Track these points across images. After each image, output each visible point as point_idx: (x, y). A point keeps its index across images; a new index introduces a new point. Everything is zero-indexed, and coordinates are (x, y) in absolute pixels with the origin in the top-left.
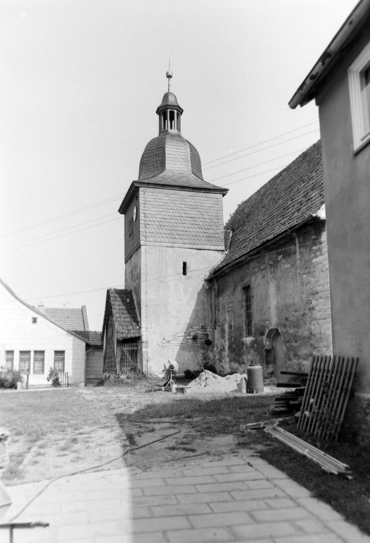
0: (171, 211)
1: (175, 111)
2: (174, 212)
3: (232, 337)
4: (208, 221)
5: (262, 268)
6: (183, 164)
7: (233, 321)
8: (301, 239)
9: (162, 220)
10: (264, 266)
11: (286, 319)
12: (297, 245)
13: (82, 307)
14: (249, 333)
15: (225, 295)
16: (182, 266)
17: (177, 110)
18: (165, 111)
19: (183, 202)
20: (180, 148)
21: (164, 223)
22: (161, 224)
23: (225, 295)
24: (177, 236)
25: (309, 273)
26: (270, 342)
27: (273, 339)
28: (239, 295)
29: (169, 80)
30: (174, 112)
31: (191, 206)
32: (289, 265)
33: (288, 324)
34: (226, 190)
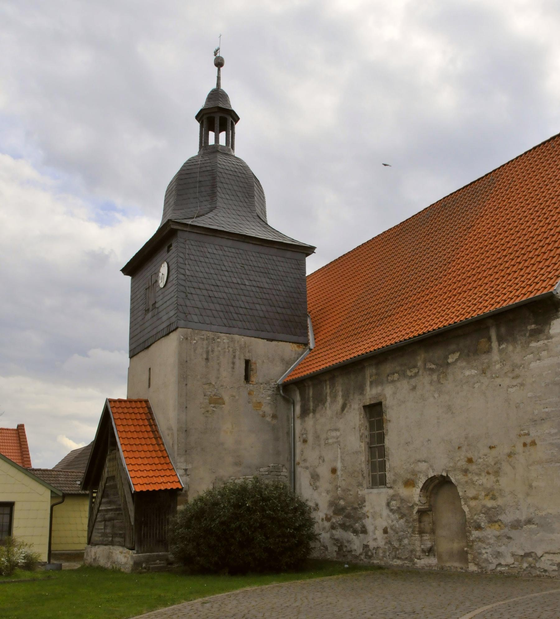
0: (226, 273)
2: (232, 275)
3: (337, 487)
4: (284, 294)
5: (409, 373)
6: (242, 200)
7: (339, 461)
8: (503, 330)
9: (213, 288)
10: (416, 370)
13: (18, 426)
16: (243, 366)
18: (212, 115)
19: (246, 262)
21: (216, 294)
22: (211, 294)
24: (235, 316)
25: (522, 385)
26: (427, 497)
28: (355, 417)
29: (219, 70)
31: (258, 269)
32: (474, 372)
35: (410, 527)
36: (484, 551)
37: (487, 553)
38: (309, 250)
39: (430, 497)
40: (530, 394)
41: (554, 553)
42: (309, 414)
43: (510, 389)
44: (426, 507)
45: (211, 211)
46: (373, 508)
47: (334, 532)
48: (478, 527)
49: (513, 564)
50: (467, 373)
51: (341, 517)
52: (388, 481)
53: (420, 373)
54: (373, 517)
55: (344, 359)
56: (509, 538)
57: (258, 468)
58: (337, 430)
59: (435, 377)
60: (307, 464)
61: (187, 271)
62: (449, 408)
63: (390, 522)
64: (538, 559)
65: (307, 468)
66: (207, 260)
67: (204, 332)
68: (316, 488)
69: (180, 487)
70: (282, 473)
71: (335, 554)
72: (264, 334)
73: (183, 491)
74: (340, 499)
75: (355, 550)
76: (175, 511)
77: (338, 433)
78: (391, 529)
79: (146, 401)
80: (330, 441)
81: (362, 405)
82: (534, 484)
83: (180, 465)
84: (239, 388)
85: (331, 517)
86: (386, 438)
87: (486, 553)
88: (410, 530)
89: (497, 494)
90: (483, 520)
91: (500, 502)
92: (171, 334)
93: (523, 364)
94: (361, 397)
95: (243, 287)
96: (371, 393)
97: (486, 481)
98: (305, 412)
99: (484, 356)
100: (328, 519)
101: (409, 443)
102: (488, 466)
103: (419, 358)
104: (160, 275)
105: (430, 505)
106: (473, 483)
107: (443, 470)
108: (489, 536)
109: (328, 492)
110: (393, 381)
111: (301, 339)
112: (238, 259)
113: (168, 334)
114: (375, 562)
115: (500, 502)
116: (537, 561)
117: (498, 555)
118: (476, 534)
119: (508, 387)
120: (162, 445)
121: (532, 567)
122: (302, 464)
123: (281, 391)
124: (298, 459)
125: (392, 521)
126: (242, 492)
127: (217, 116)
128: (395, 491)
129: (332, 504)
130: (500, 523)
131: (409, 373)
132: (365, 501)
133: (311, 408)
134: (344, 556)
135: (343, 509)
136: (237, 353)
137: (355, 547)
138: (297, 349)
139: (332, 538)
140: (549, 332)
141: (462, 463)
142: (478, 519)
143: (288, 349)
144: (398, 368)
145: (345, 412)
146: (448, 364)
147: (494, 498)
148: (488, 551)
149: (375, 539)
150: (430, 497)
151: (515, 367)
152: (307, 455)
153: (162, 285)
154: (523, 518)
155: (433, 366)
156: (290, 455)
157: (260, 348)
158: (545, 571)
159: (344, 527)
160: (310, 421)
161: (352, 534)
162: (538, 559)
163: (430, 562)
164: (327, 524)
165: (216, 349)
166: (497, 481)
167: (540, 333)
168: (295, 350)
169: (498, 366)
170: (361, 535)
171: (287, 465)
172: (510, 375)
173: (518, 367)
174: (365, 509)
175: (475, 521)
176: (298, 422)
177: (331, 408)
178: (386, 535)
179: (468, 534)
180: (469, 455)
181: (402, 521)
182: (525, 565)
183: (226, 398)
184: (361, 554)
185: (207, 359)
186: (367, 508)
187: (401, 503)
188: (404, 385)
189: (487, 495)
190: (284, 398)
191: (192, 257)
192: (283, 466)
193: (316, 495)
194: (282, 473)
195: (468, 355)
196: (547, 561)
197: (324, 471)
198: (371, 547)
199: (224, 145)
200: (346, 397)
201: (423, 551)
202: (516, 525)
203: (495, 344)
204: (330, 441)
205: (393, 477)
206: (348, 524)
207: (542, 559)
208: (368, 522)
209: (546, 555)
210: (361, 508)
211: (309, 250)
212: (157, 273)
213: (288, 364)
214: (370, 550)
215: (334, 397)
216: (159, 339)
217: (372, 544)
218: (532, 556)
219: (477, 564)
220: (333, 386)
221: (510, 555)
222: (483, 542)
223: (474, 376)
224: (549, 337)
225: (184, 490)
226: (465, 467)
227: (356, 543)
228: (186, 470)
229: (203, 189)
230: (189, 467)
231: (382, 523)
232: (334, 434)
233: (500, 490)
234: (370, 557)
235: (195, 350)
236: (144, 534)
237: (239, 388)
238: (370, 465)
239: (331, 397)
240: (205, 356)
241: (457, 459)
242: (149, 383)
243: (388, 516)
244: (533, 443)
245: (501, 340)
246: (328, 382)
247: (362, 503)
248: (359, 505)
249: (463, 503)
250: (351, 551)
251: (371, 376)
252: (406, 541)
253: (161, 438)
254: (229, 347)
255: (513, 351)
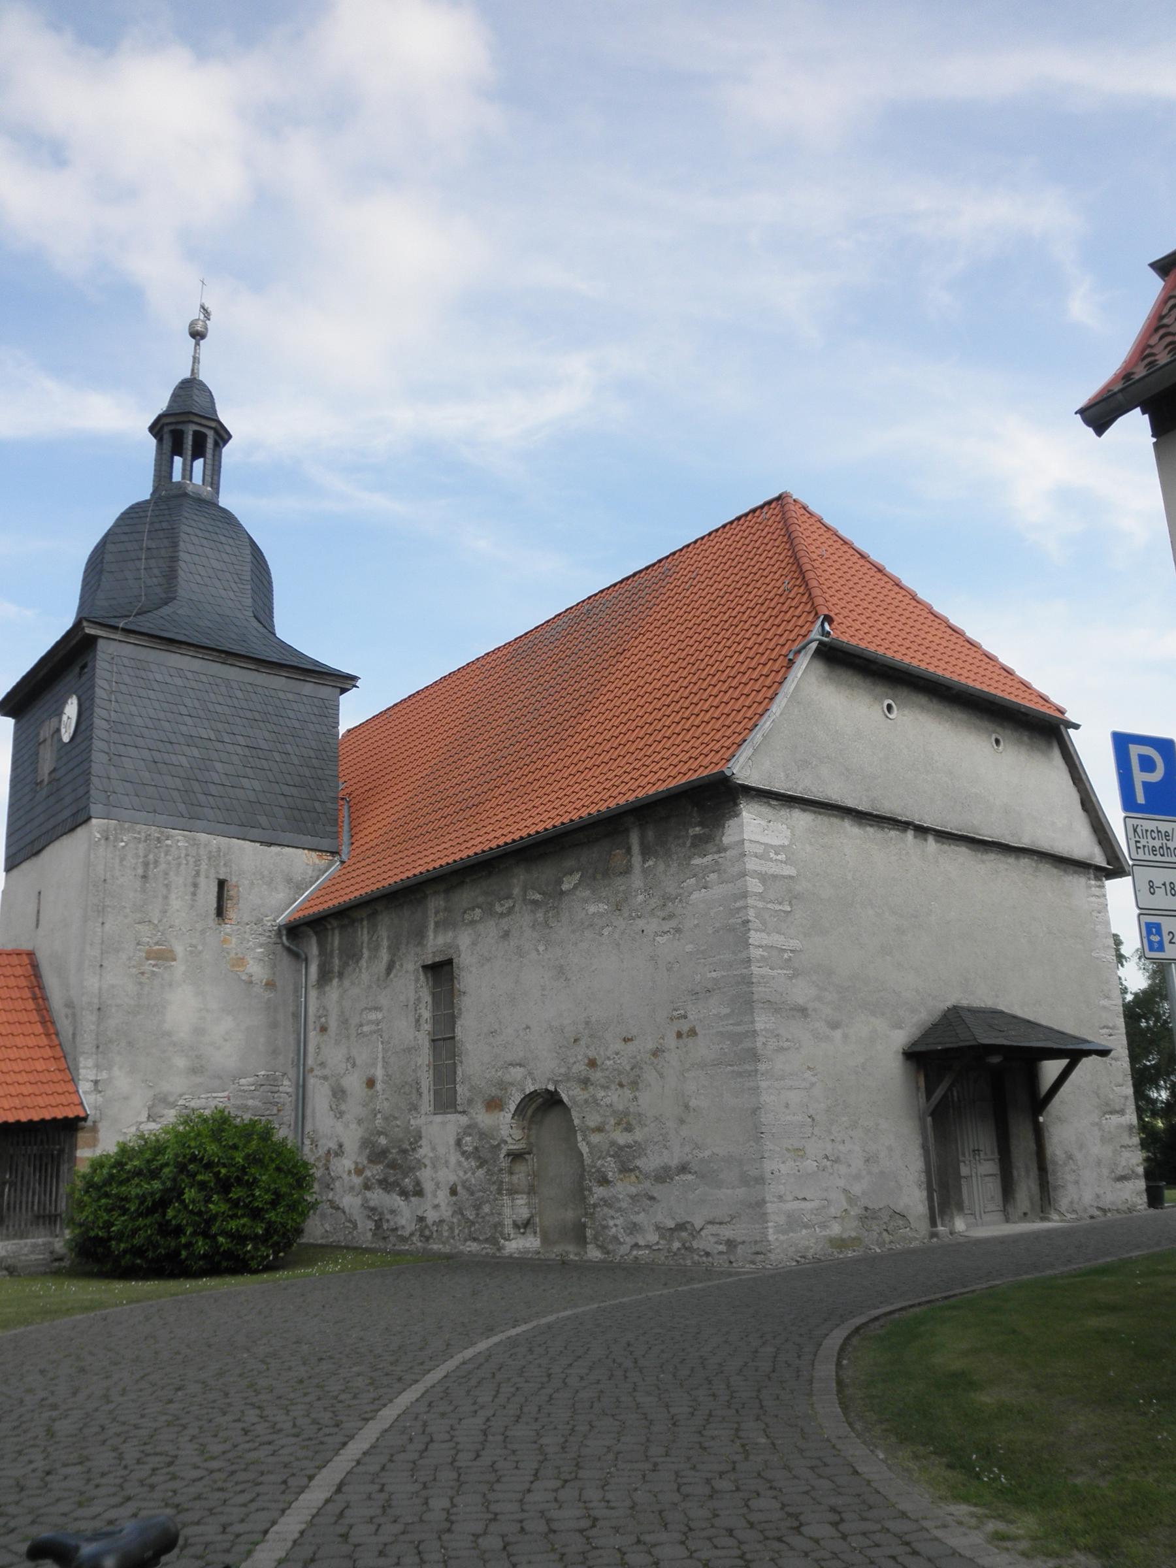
1: (211, 435)
3: (374, 1113)
4: (296, 762)
5: (498, 909)
7: (380, 1065)
8: (650, 835)
10: (510, 903)
11: (592, 1063)
12: (636, 849)
14: (446, 1102)
15: (353, 983)
16: (214, 889)
17: (215, 430)
18: (179, 427)
20: (223, 539)
23: (353, 983)
24: (202, 798)
25: (678, 930)
27: (531, 1122)
28: (410, 986)
29: (197, 344)
30: (204, 436)
32: (603, 907)
33: (597, 1075)
34: (354, 678)
35: (494, 1183)
36: (611, 1223)
37: (616, 1225)
38: (345, 682)
39: (529, 1129)
40: (689, 948)
41: (721, 1223)
42: (331, 980)
43: (658, 938)
44: (521, 1146)
45: (166, 604)
46: (434, 1149)
47: (368, 1194)
48: (604, 1181)
49: (658, 1243)
50: (592, 909)
51: (380, 1167)
52: (459, 1101)
53: (517, 909)
54: (434, 1167)
55: (391, 881)
56: (652, 1198)
57: (235, 1079)
58: (377, 1009)
59: (540, 916)
60: (327, 1072)
61: (113, 713)
62: (561, 971)
63: (461, 1174)
64: (695, 1233)
65: (325, 1078)
66: (152, 694)
67: (138, 827)
68: (340, 1115)
69: (82, 1115)
70: (281, 1089)
71: (369, 1234)
72: (256, 833)
73: (89, 1123)
74: (380, 1133)
75: (403, 1227)
76: (73, 1159)
77: (380, 1016)
78: (464, 1187)
79: (31, 954)
80: (366, 1029)
81: (420, 963)
82: (693, 1103)
83: (87, 1071)
84: (203, 932)
85: (364, 1167)
86: (459, 1023)
87: (616, 1225)
88: (494, 1188)
89: (634, 1122)
90: (610, 1167)
91: (638, 1135)
92: (79, 830)
93: (680, 895)
94: (418, 949)
95: (219, 746)
96: (435, 944)
97: (615, 1098)
98: (325, 977)
99: (619, 880)
100: (359, 1172)
101: (496, 1031)
102: (620, 1073)
103: (515, 881)
104: (65, 718)
105: (529, 1144)
106: (596, 1101)
107: (549, 1080)
108: (621, 1197)
109: (360, 1122)
110: (472, 922)
111: (326, 843)
112: (212, 695)
113: (72, 830)
114: (435, 1247)
115: (638, 1135)
116: (694, 1237)
117: (633, 1228)
118: (599, 1192)
119: (656, 934)
120: (54, 1036)
121: (686, 1249)
122: (318, 1072)
123: (284, 938)
124: (310, 1062)
125: (465, 1173)
126: (220, 1124)
127: (189, 428)
128: (471, 1118)
129: (366, 1143)
130: (637, 1173)
131: (498, 909)
132: (420, 1138)
133: (336, 969)
134: (384, 1238)
135: (384, 1153)
136: (204, 867)
137: (403, 1222)
138: (317, 861)
139: (365, 1206)
140: (721, 841)
141: (580, 1068)
142: (603, 1165)
143: (301, 861)
144: (481, 899)
145: (392, 976)
146: (562, 893)
147: (629, 1129)
148: (618, 1222)
149: (436, 1207)
150: (529, 1129)
151: (667, 898)
152: (330, 1053)
153: (66, 738)
154: (674, 1163)
155: (538, 897)
156: (298, 1054)
157: (248, 858)
158: (707, 1254)
159: (386, 1184)
160: (333, 992)
161: (398, 1198)
162: (695, 1233)
163: (528, 1245)
164: (357, 1181)
165: (162, 860)
166: (635, 1098)
167: (707, 842)
168: (315, 864)
169: (640, 898)
170: (413, 1199)
171: (292, 1073)
172: (661, 914)
173: (673, 900)
174: (422, 1152)
175: (598, 1170)
176: (313, 994)
177: (368, 970)
178: (454, 1198)
179: (587, 1193)
180: (591, 1054)
181: (481, 1173)
182: (676, 1245)
183: (179, 950)
184: (412, 1234)
185: (144, 877)
186: (424, 1151)
187: (481, 1139)
188: (490, 930)
189: (618, 1124)
190: (289, 950)
191: (123, 688)
192: (284, 1074)
193: (339, 1127)
194: (281, 1089)
195: (595, 878)
196: (710, 1238)
197: (353, 1083)
198: (430, 1221)
199: (200, 483)
200: (394, 949)
201: (516, 1226)
202: (663, 1176)
203: (637, 859)
204: (366, 1029)
205: (468, 1094)
206: (391, 1179)
207: (703, 1233)
208: (425, 1175)
209: (709, 1226)
210: (414, 1150)
211: (345, 682)
212: (59, 713)
213: (299, 888)
214: (427, 1226)
215: (375, 949)
216: (58, 838)
217: (431, 1216)
218: (686, 1229)
219: (601, 1247)
220: (373, 929)
221: (652, 1228)
222: (610, 1206)
223: (601, 915)
224: (722, 849)
225: (90, 1118)
226: (584, 1074)
227: (404, 1214)
228: (96, 1082)
229: (153, 563)
230: (104, 1075)
231: (448, 1176)
232: (373, 1016)
233: (640, 1115)
234: (428, 1239)
235: (122, 860)
236: (9, 1204)
237: (203, 932)
238: (431, 1072)
239: (369, 949)
240: (140, 871)
241: (572, 1061)
242: (38, 920)
243: (459, 1163)
244: (693, 1033)
245: (646, 852)
246: (365, 923)
247: (417, 1142)
248: (411, 1144)
249: (579, 1138)
250: (396, 1229)
251: (436, 913)
252: (486, 1209)
253: (53, 1023)
254: (187, 855)
255: (665, 872)
